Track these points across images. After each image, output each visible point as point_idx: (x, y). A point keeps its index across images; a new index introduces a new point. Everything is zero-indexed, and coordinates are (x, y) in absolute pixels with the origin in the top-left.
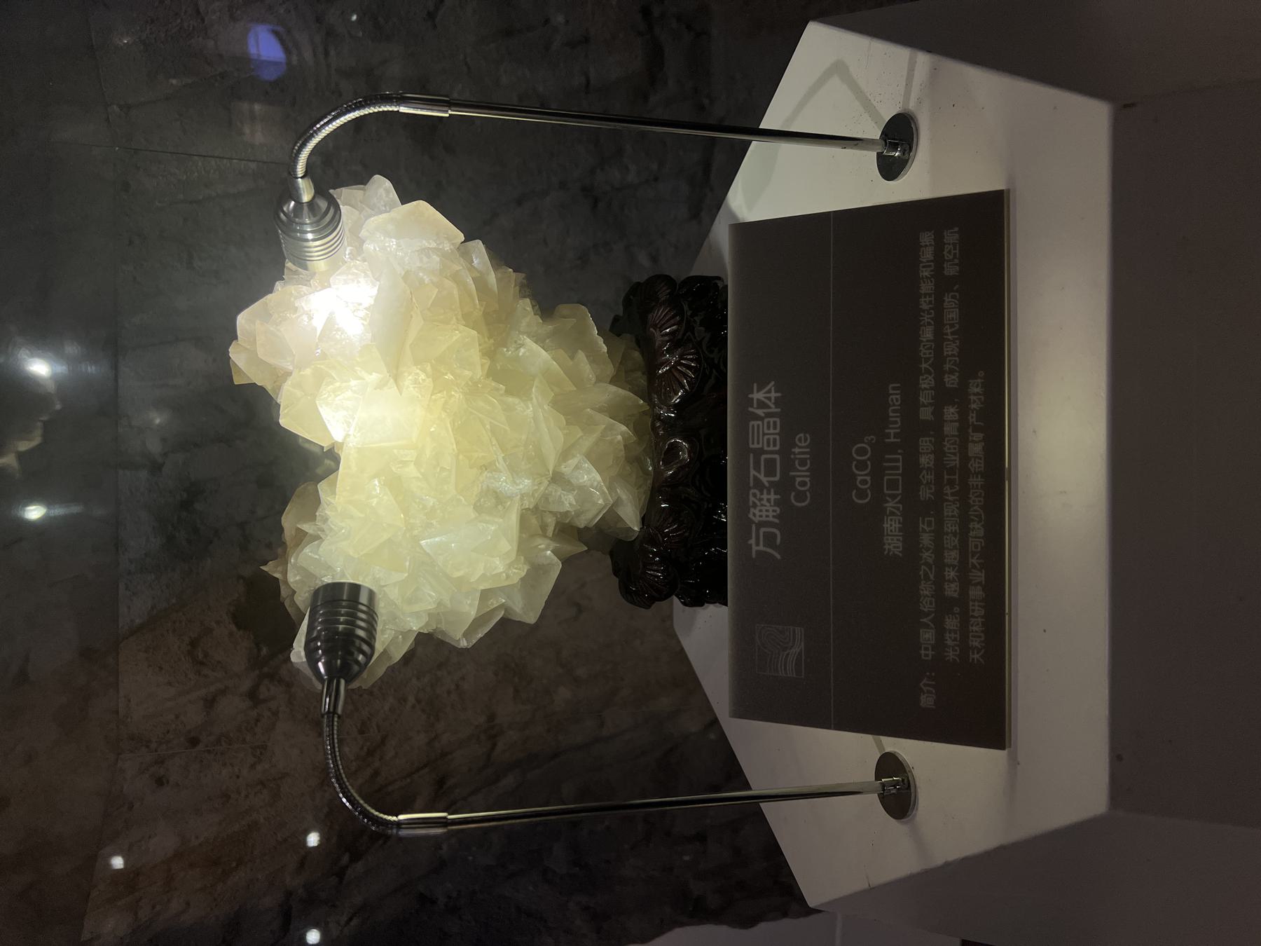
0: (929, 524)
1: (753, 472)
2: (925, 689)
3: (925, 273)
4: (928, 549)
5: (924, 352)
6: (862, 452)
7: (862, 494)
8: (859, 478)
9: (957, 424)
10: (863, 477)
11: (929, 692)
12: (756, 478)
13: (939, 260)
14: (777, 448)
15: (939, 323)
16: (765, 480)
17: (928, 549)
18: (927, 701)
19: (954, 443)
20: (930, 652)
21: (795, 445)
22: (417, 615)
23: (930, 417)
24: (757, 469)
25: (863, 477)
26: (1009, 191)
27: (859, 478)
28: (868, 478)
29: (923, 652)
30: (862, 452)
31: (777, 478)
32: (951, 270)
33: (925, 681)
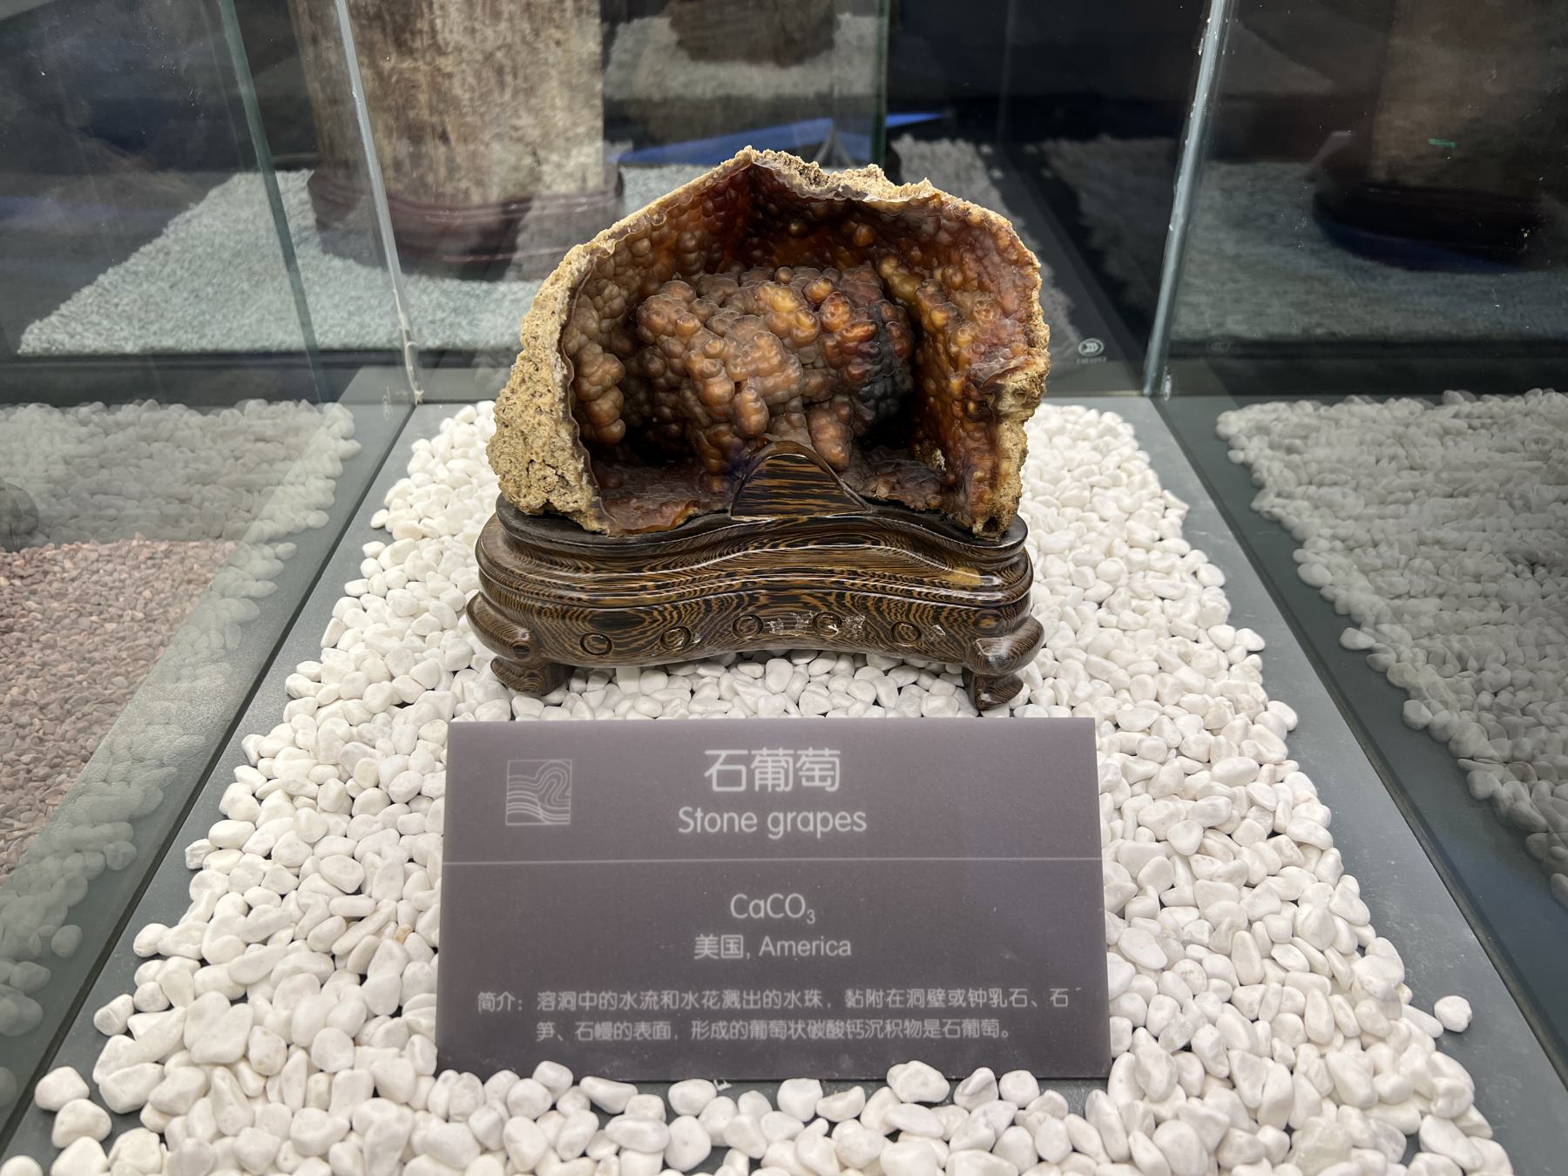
0: (1019, 1001)
1: (724, 753)
2: (501, 998)
3: (667, 998)
4: (638, 1001)
5: (915, 996)
6: (795, 906)
7: (742, 907)
8: (762, 903)
9: (783, 1037)
10: (763, 908)
11: (498, 1004)
12: (717, 757)
13: (711, 1016)
14: (804, 783)
15: (747, 1015)
16: (713, 771)
17: (638, 1001)
18: (487, 1001)
19: (624, 1035)
20: (588, 1004)
21: (705, 813)
22: (1453, 402)
23: (543, 1006)
24: (730, 760)
25: (763, 908)
26: (713, 1138)
27: (762, 903)
28: (762, 914)
29: (588, 994)
30: (795, 906)
31: (716, 788)
32: (697, 1028)
33: (511, 998)
